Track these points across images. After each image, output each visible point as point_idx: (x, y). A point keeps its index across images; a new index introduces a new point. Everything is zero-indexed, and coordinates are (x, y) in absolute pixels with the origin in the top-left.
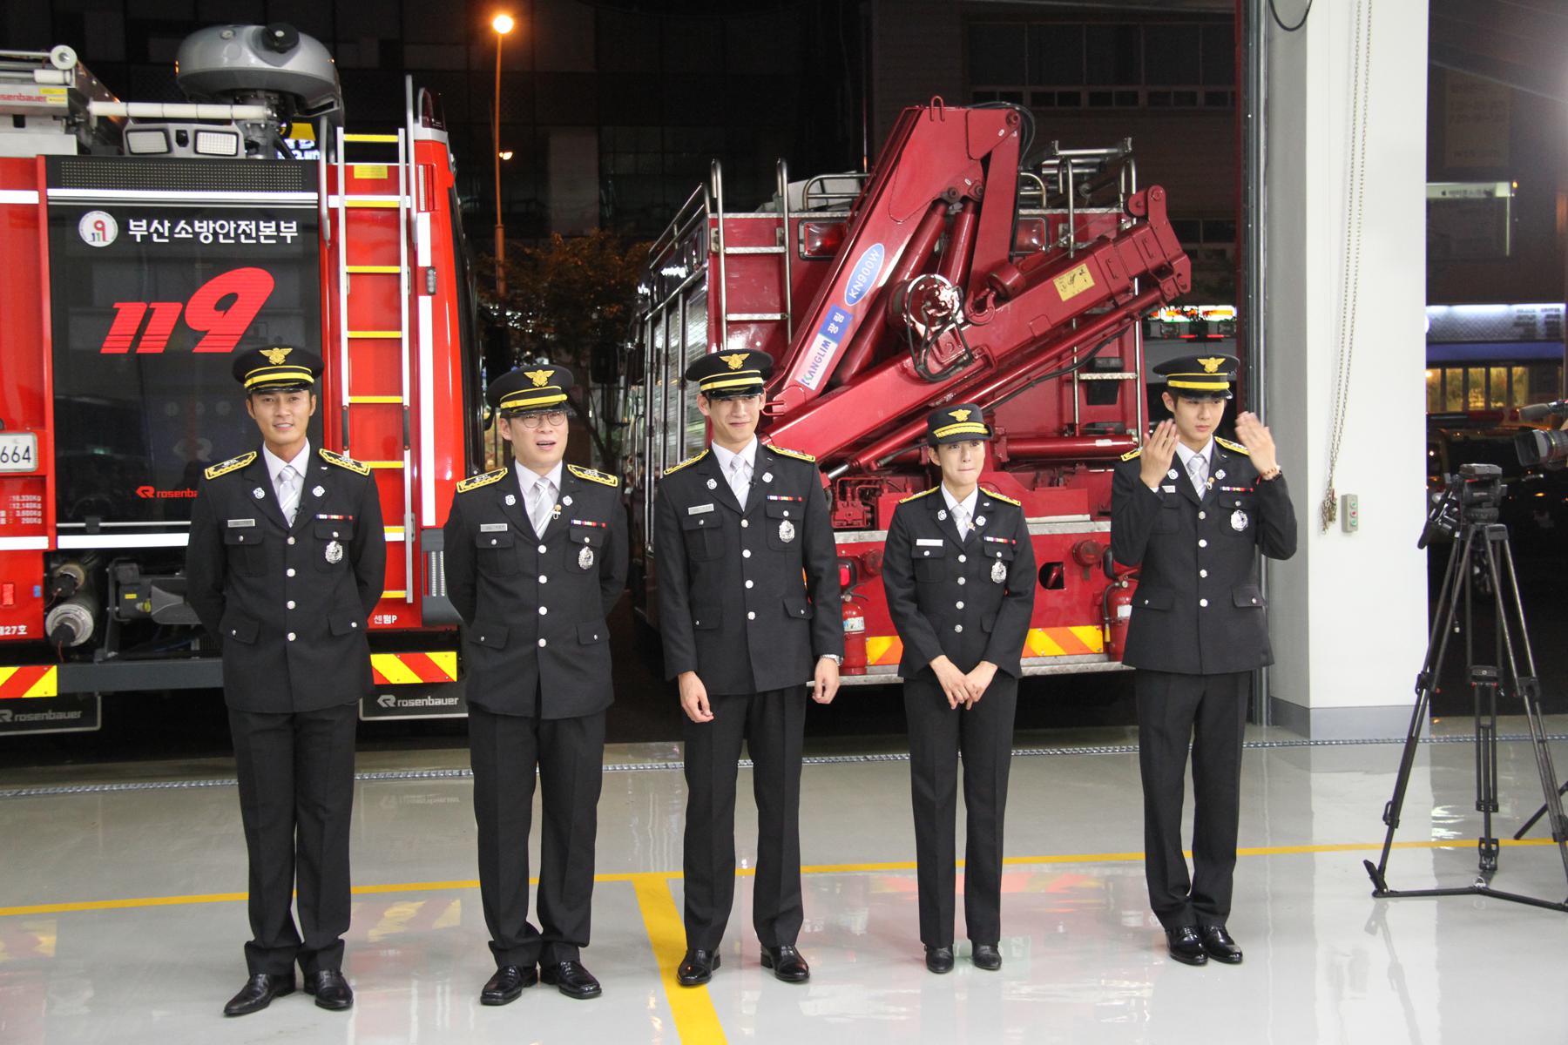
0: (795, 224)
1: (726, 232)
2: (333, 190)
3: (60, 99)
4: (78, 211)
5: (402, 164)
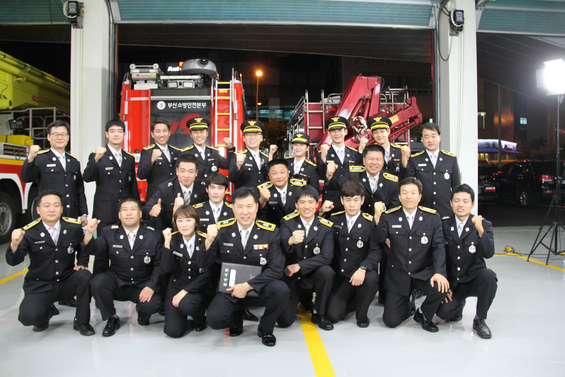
0: (325, 105)
1: (307, 106)
2: (214, 95)
3: (154, 76)
4: (155, 102)
5: (230, 89)
